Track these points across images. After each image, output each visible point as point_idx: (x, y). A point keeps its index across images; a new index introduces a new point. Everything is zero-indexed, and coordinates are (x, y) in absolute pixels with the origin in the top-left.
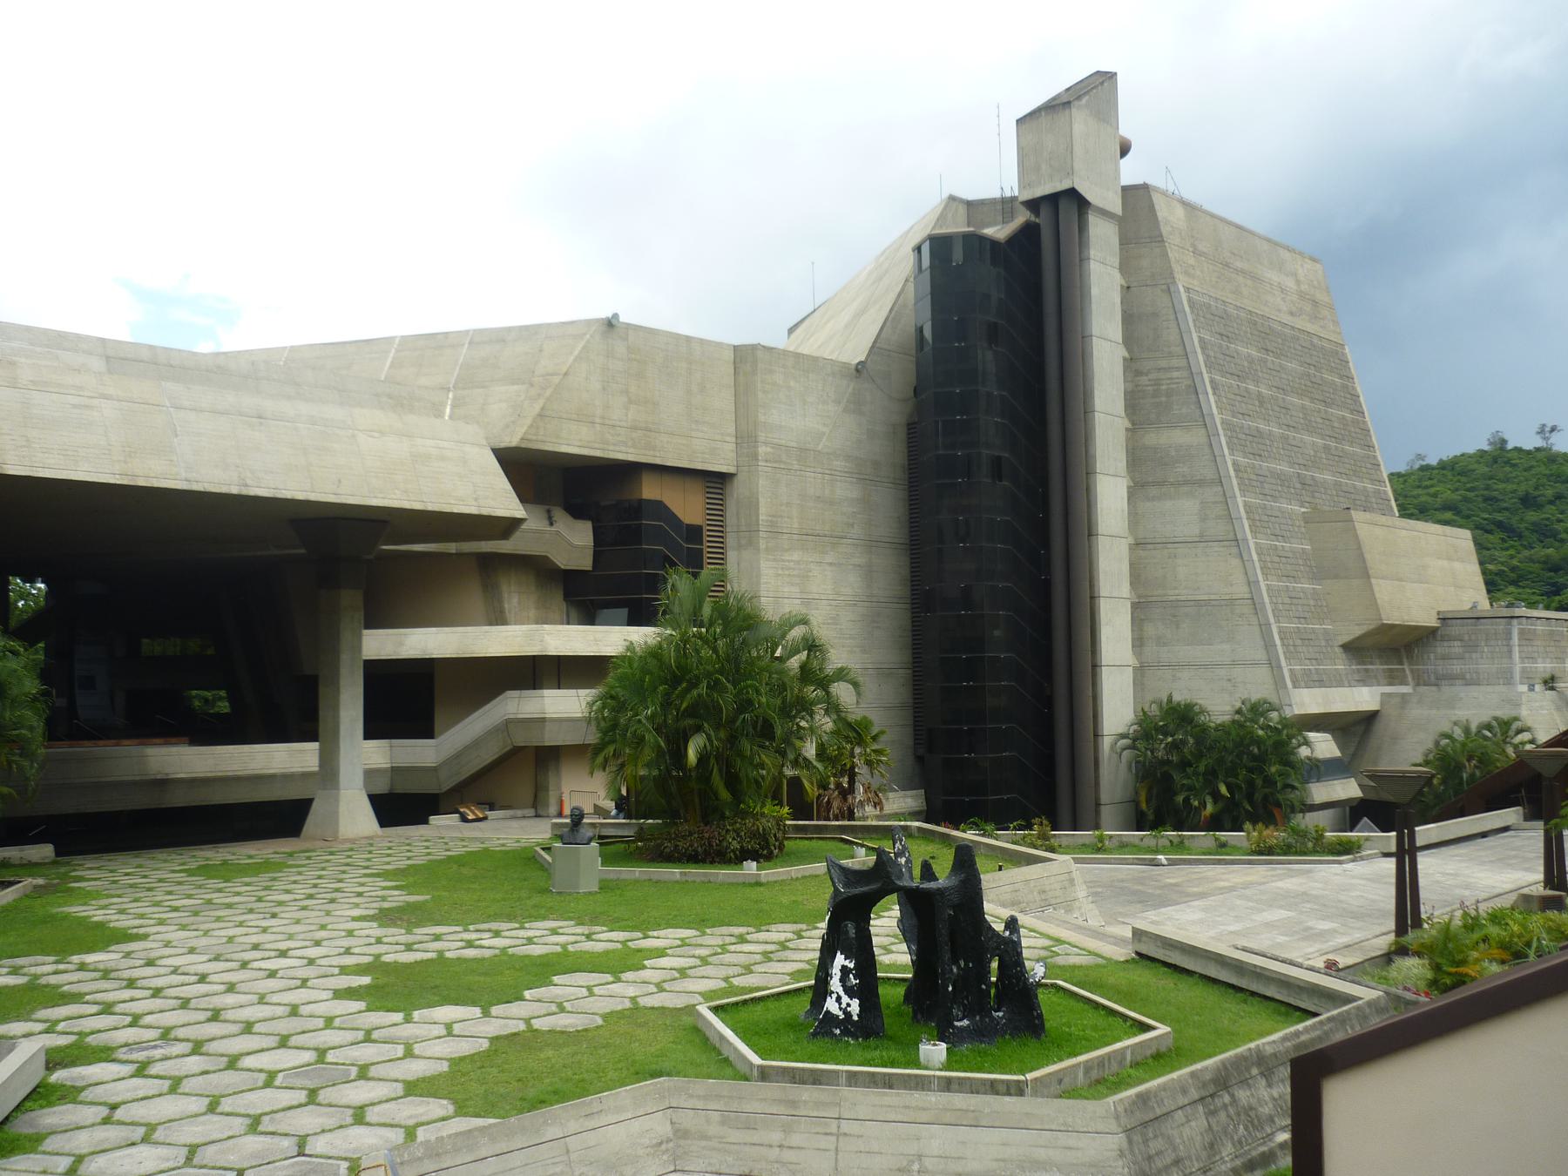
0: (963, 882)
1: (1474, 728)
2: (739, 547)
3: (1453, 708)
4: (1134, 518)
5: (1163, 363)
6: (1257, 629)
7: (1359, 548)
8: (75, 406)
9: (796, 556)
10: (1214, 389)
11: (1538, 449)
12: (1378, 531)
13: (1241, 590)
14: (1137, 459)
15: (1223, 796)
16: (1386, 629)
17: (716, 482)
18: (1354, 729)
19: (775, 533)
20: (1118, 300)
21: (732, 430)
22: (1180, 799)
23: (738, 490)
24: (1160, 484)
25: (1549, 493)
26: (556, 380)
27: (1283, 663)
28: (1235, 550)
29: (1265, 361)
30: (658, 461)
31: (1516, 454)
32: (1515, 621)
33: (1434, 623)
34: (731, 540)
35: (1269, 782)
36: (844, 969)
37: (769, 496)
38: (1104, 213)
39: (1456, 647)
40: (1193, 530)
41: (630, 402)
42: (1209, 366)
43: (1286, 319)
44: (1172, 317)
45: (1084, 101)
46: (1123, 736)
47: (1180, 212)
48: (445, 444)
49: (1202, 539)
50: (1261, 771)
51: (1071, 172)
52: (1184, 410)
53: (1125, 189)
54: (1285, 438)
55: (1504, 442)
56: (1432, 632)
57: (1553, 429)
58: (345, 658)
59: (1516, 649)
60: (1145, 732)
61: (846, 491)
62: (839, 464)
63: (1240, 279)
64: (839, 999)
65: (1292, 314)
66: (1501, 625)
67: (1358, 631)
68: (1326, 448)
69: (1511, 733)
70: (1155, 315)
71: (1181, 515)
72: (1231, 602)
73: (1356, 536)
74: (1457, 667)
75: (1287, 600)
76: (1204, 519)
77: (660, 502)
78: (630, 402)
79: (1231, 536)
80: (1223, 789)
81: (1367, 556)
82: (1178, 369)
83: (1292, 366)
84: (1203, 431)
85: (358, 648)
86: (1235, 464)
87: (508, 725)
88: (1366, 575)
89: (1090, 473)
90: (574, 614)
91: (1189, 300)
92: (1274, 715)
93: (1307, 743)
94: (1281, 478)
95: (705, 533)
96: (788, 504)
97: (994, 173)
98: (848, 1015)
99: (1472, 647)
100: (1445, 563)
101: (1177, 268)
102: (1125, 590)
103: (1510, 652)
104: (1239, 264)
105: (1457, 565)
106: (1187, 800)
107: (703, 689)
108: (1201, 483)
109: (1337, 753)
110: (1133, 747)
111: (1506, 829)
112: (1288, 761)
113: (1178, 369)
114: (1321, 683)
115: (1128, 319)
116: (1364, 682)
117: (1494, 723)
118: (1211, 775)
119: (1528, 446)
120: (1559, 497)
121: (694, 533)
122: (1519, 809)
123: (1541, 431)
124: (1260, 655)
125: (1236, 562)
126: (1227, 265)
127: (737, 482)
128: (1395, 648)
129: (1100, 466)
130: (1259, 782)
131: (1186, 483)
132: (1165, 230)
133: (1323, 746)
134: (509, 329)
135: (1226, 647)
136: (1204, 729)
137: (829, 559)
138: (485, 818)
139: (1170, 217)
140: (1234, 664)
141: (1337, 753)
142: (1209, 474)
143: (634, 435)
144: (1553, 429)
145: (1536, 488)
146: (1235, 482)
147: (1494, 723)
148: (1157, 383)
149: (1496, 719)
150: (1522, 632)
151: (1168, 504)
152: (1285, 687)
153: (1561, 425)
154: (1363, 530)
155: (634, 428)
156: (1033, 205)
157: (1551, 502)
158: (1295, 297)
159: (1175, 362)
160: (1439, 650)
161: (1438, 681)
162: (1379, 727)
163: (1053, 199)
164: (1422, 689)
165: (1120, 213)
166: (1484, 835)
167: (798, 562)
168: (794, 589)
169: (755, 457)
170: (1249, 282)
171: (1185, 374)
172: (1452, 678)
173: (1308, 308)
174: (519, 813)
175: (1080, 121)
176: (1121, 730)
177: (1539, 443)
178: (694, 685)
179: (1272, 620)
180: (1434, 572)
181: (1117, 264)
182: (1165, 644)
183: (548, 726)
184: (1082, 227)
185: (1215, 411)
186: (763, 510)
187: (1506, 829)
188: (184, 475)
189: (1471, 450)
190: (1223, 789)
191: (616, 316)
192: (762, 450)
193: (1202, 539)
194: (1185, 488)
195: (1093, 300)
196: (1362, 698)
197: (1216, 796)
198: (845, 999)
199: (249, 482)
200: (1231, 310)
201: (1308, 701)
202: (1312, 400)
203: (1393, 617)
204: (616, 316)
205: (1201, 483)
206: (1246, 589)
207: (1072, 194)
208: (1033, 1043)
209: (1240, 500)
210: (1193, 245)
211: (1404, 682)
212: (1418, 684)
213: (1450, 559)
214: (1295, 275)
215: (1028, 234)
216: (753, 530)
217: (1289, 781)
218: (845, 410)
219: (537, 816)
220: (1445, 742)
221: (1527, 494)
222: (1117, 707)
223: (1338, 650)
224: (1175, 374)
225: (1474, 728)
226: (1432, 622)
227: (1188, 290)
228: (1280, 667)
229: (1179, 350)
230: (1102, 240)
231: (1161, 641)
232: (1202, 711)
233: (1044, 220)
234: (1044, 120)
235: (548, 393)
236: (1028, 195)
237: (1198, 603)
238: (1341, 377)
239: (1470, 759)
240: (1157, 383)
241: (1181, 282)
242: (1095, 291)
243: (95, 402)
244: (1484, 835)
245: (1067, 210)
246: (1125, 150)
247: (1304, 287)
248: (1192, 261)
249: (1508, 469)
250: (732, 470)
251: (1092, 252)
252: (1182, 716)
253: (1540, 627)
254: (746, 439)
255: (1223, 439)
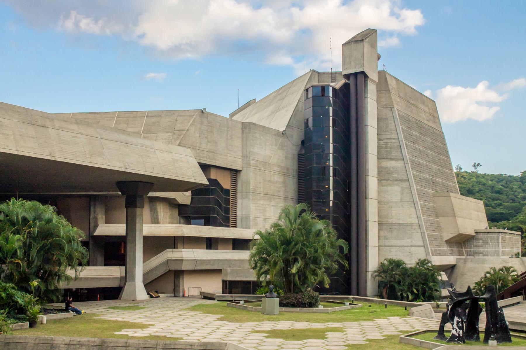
0: (491, 296)
1: (497, 270)
2: (242, 198)
3: (484, 264)
4: (379, 192)
5: (389, 137)
6: (420, 234)
7: (452, 206)
8: (73, 137)
9: (262, 202)
10: (407, 147)
11: (473, 172)
12: (458, 200)
13: (415, 220)
14: (380, 171)
15: (415, 293)
16: (460, 235)
17: (235, 173)
18: (450, 269)
19: (255, 193)
20: (376, 113)
21: (241, 155)
22: (399, 294)
23: (242, 177)
24: (387, 180)
25: (477, 189)
26: (184, 132)
27: (429, 246)
28: (413, 205)
29: (420, 137)
30: (217, 165)
31: (465, 174)
32: (500, 234)
33: (474, 234)
34: (239, 195)
35: (430, 289)
36: (458, 322)
37: (251, 178)
38: (373, 81)
39: (480, 243)
40: (399, 198)
41: (208, 142)
42: (406, 138)
43: (426, 122)
44: (393, 120)
45: (367, 40)
46: (375, 271)
47: (394, 82)
48: (181, 156)
49: (401, 201)
50: (428, 285)
51: (363, 66)
52: (396, 154)
53: (379, 72)
54: (427, 165)
55: (461, 168)
56: (473, 237)
57: (478, 165)
58: (138, 233)
59: (500, 244)
60: (383, 270)
61: (278, 178)
62: (276, 168)
63: (413, 107)
64: (456, 330)
65: (428, 120)
66: (496, 235)
67: (451, 236)
68: (439, 170)
69: (510, 272)
70: (387, 119)
71: (394, 192)
72: (411, 224)
73: (451, 202)
74: (481, 250)
75: (429, 224)
76: (402, 194)
77: (216, 180)
78: (208, 142)
79: (412, 200)
80: (415, 291)
81: (455, 209)
82: (394, 139)
83: (428, 139)
84: (402, 162)
85: (141, 230)
86: (413, 174)
87: (168, 262)
88: (454, 216)
89: (366, 175)
90: (182, 221)
91: (399, 114)
92: (430, 265)
93: (440, 275)
94: (426, 179)
95: (231, 192)
96: (260, 183)
97: (332, 60)
98: (459, 335)
99: (486, 242)
100: (476, 213)
101: (394, 102)
102: (376, 219)
103: (499, 245)
104: (412, 102)
105: (480, 213)
106: (402, 294)
107: (299, 246)
108: (401, 181)
109: (455, 317)
110: (378, 276)
111: (518, 303)
112: (435, 281)
113: (394, 139)
114: (440, 254)
115: (379, 120)
116: (452, 254)
117: (504, 269)
118: (410, 286)
119: (470, 171)
120: (480, 190)
121: (227, 191)
122: (522, 296)
123: (474, 166)
124: (421, 243)
125: (413, 210)
126: (408, 102)
127: (242, 174)
128: (462, 242)
129: (370, 173)
130: (427, 289)
131: (397, 180)
132: (390, 88)
133: (443, 277)
134: (163, 111)
135: (409, 240)
136: (405, 269)
137: (273, 203)
138: (159, 297)
139: (392, 83)
140: (411, 246)
141: (455, 317)
142: (405, 178)
143: (209, 154)
144: (478, 165)
145: (473, 187)
146: (413, 180)
147: (504, 269)
148: (386, 143)
149: (505, 267)
150: (502, 237)
151: (389, 188)
152: (429, 255)
153: (481, 164)
154: (454, 200)
155: (209, 152)
156: (347, 76)
157: (478, 192)
158: (428, 115)
159: (393, 136)
160: (475, 244)
161: (474, 254)
162: (456, 270)
163: (356, 75)
164: (469, 257)
165: (377, 81)
166: (513, 305)
167: (262, 205)
168: (262, 215)
169: (249, 164)
170: (415, 108)
171: (397, 141)
172: (479, 253)
173: (432, 118)
174: (169, 295)
175: (366, 46)
176: (373, 270)
177: (473, 170)
178: (296, 244)
179: (425, 231)
180: (472, 216)
181: (376, 100)
182: (387, 239)
183: (184, 262)
184: (366, 86)
185: (407, 155)
186: (251, 185)
187: (518, 303)
188: (108, 164)
189: (515, 175)
190: (415, 291)
191: (205, 109)
192: (252, 162)
193: (401, 201)
194: (396, 182)
195: (369, 112)
196: (450, 260)
197: (412, 293)
198: (458, 330)
199: (127, 167)
200: (411, 119)
201: (437, 260)
202: (435, 152)
203: (463, 232)
204: (205, 109)
205: (401, 181)
206: (417, 220)
207: (363, 73)
208: (508, 343)
209: (415, 187)
210: (399, 94)
211: (463, 255)
212: (467, 256)
213: (477, 211)
214: (428, 106)
215: (346, 86)
216: (248, 192)
217: (436, 288)
218: (279, 148)
219: (175, 296)
220: (488, 275)
221: (469, 189)
222: (373, 261)
223: (445, 243)
224: (393, 141)
225: (497, 270)
226: (471, 232)
227: (398, 110)
228: (428, 248)
229: (395, 132)
230: (372, 89)
231: (386, 238)
232: (404, 263)
233: (351, 82)
234: (353, 45)
235: (182, 137)
236: (344, 73)
237: (400, 224)
238: (443, 144)
239: (500, 281)
240: (386, 143)
241: (396, 107)
242: (369, 109)
243: (79, 135)
244: (513, 305)
245: (360, 78)
246: (379, 58)
247: (431, 111)
248: (398, 100)
249: (462, 179)
250: (240, 169)
251: (369, 95)
252: (398, 264)
253: (507, 236)
254: (245, 158)
255: (410, 165)
